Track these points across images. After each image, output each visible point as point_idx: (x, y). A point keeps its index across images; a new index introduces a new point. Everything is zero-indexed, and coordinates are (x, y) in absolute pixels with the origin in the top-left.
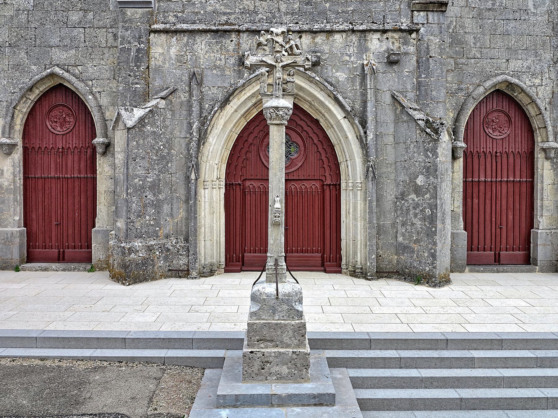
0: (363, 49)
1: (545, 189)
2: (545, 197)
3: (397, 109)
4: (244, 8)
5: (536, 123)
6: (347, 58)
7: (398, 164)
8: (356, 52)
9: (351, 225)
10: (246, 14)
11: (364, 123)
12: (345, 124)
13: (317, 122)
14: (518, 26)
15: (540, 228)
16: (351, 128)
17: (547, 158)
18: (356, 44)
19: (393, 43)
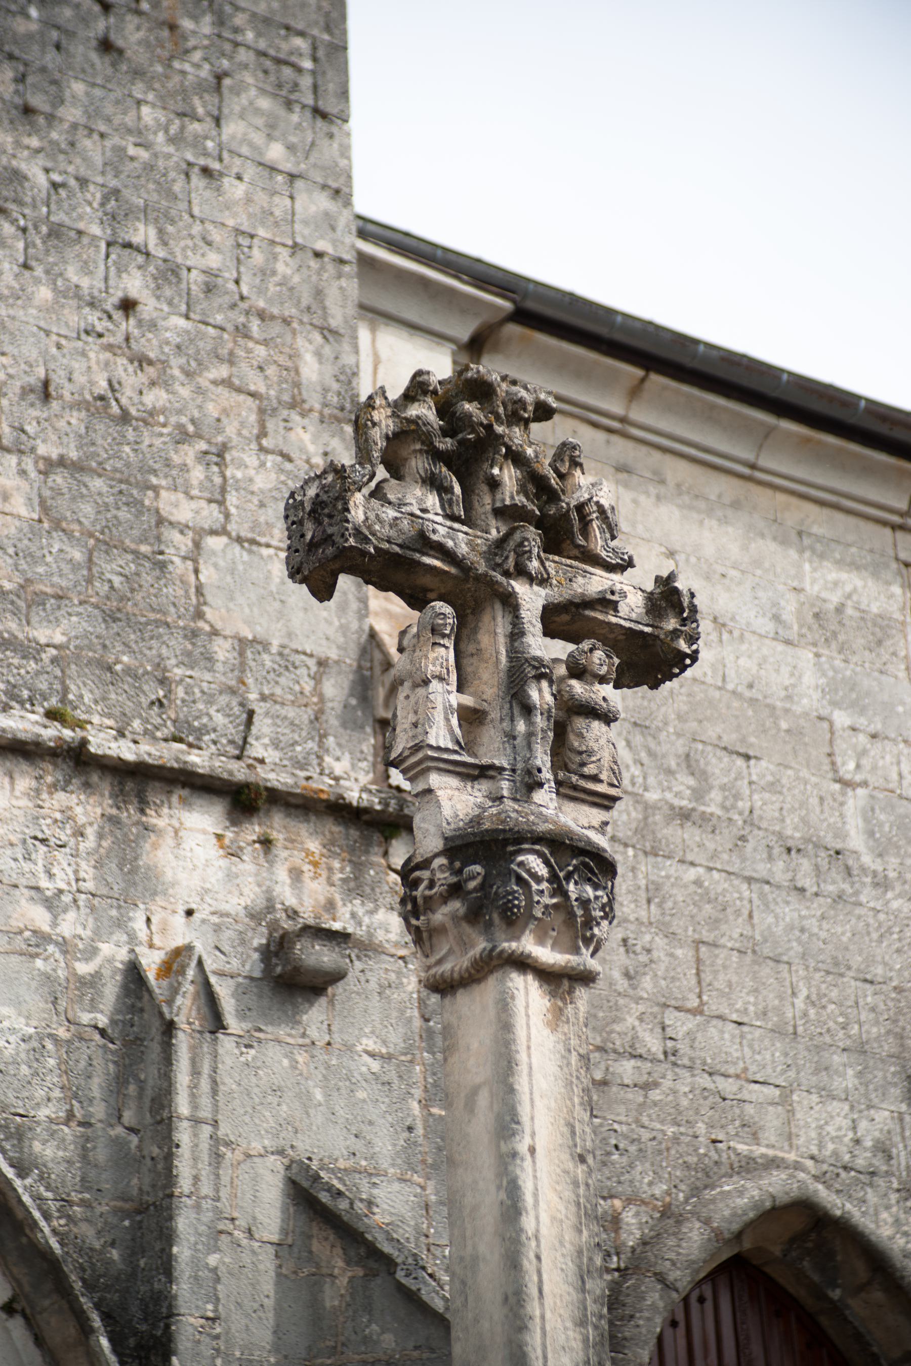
0: (129, 879)
6: (40, 917)
8: (89, 885)
14: (812, 924)
18: (90, 842)
19: (296, 874)
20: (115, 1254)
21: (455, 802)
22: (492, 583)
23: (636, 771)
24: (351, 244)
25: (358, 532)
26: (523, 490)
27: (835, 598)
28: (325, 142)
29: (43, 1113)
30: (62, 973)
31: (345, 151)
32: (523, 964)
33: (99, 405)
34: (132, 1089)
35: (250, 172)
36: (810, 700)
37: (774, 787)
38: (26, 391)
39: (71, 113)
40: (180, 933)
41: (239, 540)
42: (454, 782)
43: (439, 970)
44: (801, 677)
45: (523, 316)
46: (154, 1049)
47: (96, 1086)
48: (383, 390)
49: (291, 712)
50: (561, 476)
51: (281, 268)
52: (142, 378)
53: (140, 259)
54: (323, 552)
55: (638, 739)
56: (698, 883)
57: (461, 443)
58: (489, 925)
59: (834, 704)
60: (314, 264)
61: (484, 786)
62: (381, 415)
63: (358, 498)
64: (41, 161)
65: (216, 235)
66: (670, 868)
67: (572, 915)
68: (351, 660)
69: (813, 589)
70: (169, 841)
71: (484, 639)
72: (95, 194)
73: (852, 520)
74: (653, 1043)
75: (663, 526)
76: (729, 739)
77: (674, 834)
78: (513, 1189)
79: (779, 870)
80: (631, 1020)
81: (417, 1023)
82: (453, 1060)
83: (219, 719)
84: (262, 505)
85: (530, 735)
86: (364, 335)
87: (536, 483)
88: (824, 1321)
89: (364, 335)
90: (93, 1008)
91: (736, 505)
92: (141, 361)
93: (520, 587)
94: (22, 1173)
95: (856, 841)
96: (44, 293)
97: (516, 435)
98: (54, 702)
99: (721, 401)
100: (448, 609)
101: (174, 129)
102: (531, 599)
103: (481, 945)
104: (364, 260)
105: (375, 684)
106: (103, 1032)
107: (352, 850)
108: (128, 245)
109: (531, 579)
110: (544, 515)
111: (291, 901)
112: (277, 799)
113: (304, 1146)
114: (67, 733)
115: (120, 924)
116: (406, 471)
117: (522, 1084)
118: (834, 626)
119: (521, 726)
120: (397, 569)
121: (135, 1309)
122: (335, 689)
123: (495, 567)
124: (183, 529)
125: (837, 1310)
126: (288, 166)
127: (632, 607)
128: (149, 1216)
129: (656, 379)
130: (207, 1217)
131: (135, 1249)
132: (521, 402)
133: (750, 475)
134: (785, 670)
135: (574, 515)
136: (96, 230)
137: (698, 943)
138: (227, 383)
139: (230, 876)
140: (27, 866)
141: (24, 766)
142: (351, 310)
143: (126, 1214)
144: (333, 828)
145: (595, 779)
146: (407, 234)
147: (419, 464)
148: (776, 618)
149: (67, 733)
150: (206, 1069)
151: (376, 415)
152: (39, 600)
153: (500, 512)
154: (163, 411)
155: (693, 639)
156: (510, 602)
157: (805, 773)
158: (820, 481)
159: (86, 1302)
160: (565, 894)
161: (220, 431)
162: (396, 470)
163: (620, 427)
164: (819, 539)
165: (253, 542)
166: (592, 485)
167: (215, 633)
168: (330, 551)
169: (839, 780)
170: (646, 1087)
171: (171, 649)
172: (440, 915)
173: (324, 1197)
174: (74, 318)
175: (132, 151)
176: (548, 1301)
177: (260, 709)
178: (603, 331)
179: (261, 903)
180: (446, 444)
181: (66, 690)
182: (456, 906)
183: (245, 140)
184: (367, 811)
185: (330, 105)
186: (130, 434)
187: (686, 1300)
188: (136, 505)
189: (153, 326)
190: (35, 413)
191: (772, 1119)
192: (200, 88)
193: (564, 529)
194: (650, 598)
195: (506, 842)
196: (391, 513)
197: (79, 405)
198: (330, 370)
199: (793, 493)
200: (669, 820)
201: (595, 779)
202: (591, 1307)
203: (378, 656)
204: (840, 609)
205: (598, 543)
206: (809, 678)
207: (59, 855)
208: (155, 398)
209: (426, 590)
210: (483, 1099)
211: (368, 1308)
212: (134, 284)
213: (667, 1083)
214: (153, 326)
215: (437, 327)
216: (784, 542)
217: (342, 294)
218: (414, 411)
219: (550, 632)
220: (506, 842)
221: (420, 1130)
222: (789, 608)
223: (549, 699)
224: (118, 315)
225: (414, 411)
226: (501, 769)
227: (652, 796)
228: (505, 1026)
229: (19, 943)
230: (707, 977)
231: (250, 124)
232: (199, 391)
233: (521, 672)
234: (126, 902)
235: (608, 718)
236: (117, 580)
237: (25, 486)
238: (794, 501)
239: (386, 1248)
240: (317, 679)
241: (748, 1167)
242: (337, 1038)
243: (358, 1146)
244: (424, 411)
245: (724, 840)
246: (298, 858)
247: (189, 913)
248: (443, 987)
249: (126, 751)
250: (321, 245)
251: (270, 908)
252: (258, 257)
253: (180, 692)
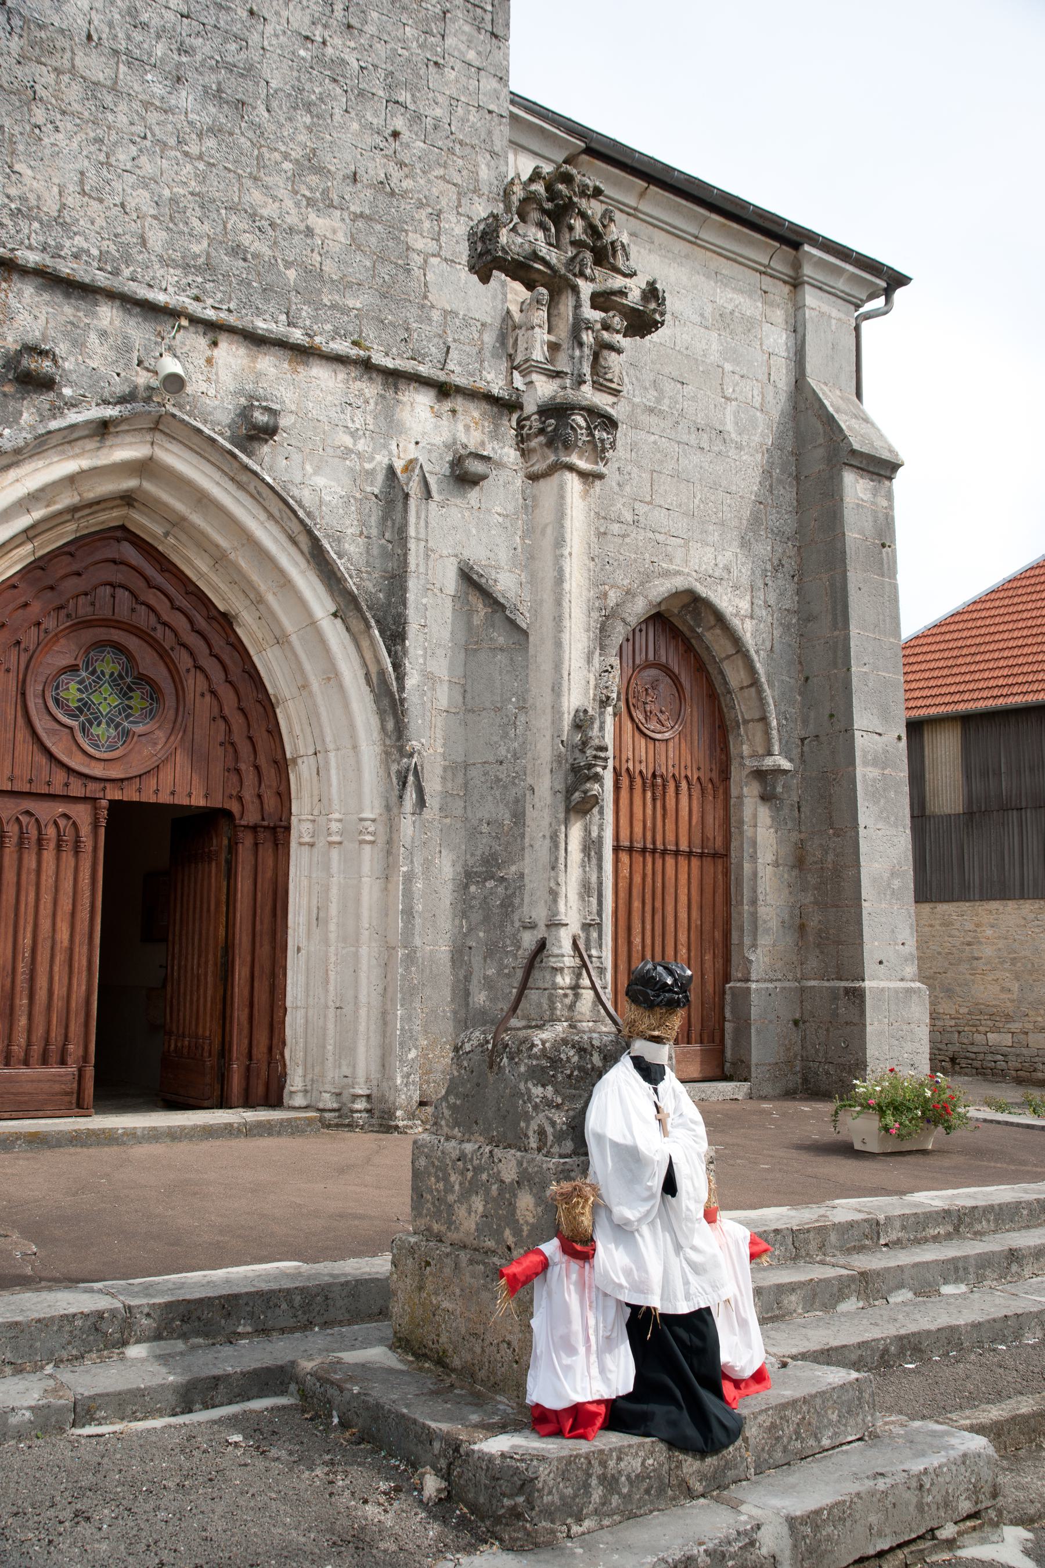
0: (390, 426)
1: (760, 875)
2: (761, 897)
3: (471, 612)
4: (23, 199)
5: (743, 708)
6: (348, 441)
7: (473, 772)
8: (371, 427)
9: (333, 959)
10: (30, 218)
11: (395, 636)
12: (334, 633)
13: (226, 621)
14: (706, 465)
15: (754, 976)
16: (351, 648)
17: (764, 798)
18: (372, 406)
19: (467, 428)
20: (381, 595)
21: (544, 389)
22: (567, 279)
23: (630, 387)
24: (505, 107)
25: (503, 249)
26: (585, 232)
27: (730, 307)
28: (495, 51)
29: (349, 531)
30: (358, 468)
31: (506, 57)
32: (571, 468)
33: (381, 185)
34: (389, 523)
35: (458, 65)
36: (714, 357)
37: (694, 399)
38: (345, 177)
39: (371, 29)
40: (412, 453)
41: (446, 260)
42: (543, 378)
43: (532, 469)
44: (711, 345)
45: (590, 151)
46: (400, 506)
47: (374, 520)
48: (518, 176)
49: (467, 348)
50: (604, 226)
51: (471, 118)
52: (402, 173)
53: (403, 110)
54: (487, 259)
55: (632, 372)
56: (655, 443)
57: (557, 205)
58: (557, 448)
59: (725, 359)
60: (488, 116)
61: (558, 381)
62: (517, 189)
63: (504, 232)
64: (355, 54)
65: (440, 99)
66: (643, 435)
67: (596, 446)
68: (497, 324)
69: (720, 302)
70: (408, 408)
71: (562, 308)
72: (381, 74)
73: (741, 267)
74: (628, 517)
75: (651, 258)
76: (674, 374)
77: (645, 419)
78: (560, 571)
79: (693, 439)
80: (619, 506)
81: (521, 501)
82: (537, 511)
83: (433, 350)
84: (457, 242)
85: (581, 357)
86: (511, 156)
87: (593, 230)
88: (693, 641)
89: (511, 156)
90: (372, 485)
91: (687, 256)
92: (402, 164)
93: (581, 282)
94: (340, 557)
95: (730, 427)
96: (355, 126)
97: (583, 203)
98: (355, 337)
99: (684, 202)
100: (545, 291)
101: (421, 40)
102: (586, 289)
103: (552, 458)
104: (513, 117)
105: (508, 331)
106: (376, 496)
107: (494, 418)
108: (397, 102)
109: (587, 278)
110: (595, 246)
111: (465, 440)
112: (459, 390)
113: (466, 554)
114: (362, 353)
115: (385, 446)
116: (528, 219)
117: (568, 523)
118: (728, 321)
119: (577, 353)
120: (522, 270)
121: (390, 620)
122: (489, 338)
123: (570, 271)
124: (419, 253)
125: (699, 637)
126: (477, 64)
127: (634, 297)
128: (396, 581)
129: (653, 188)
130: (422, 582)
131: (390, 594)
132: (587, 186)
133: (695, 241)
134: (704, 341)
135: (609, 247)
136: (381, 93)
137: (653, 471)
138: (442, 177)
139: (436, 427)
140: (342, 416)
141: (341, 367)
142: (505, 143)
143: (386, 579)
144: (485, 406)
145: (611, 381)
146: (535, 103)
147: (535, 215)
148: (702, 315)
149: (362, 353)
150: (423, 516)
151: (515, 189)
152: (349, 285)
153: (573, 243)
154: (411, 191)
155: (662, 314)
156: (575, 290)
157: (709, 393)
158: (728, 247)
159: (368, 615)
160: (593, 436)
161: (438, 203)
162: (523, 218)
163: (633, 213)
164: (725, 276)
165: (453, 261)
166: (619, 232)
167: (433, 307)
168: (489, 258)
169: (724, 397)
170: (624, 536)
171: (411, 313)
172: (534, 443)
173: (475, 577)
174: (371, 139)
175: (400, 51)
176: (573, 620)
177: (453, 346)
178: (628, 161)
179: (450, 441)
180: (548, 206)
181: (361, 331)
182: (541, 439)
183: (456, 48)
184: (501, 399)
185: (499, 31)
186: (395, 203)
187: (634, 630)
188: (396, 239)
189: (408, 146)
190: (349, 189)
191: (679, 554)
192: (435, 17)
193: (604, 254)
194: (643, 292)
195: (567, 409)
196: (520, 240)
197: (370, 186)
198: (493, 174)
199: (714, 252)
200: (643, 412)
201: (611, 381)
202: (593, 624)
203: (510, 322)
204: (732, 313)
205: (620, 262)
206: (715, 346)
207: (357, 411)
208: (408, 184)
209: (535, 281)
210: (549, 530)
211: (493, 626)
212: (399, 123)
213: (633, 535)
214: (408, 146)
215: (547, 155)
216: (708, 277)
217: (502, 133)
218: (534, 187)
219: (594, 307)
220: (567, 409)
221: (519, 550)
222: (708, 310)
223: (592, 340)
224: (391, 139)
225: (534, 187)
226: (566, 374)
227: (637, 400)
228: (562, 496)
229: (339, 452)
230: (655, 487)
231: (460, 38)
232: (429, 181)
233: (579, 325)
234: (388, 436)
235: (619, 351)
236: (387, 277)
237: (344, 226)
238: (715, 256)
239: (502, 601)
240: (481, 332)
241: (666, 574)
242: (483, 506)
243: (491, 555)
244: (539, 187)
245: (669, 423)
246: (468, 420)
247: (417, 443)
248: (534, 477)
249: (390, 363)
250: (491, 107)
251: (455, 443)
252: (460, 111)
253: (415, 336)
